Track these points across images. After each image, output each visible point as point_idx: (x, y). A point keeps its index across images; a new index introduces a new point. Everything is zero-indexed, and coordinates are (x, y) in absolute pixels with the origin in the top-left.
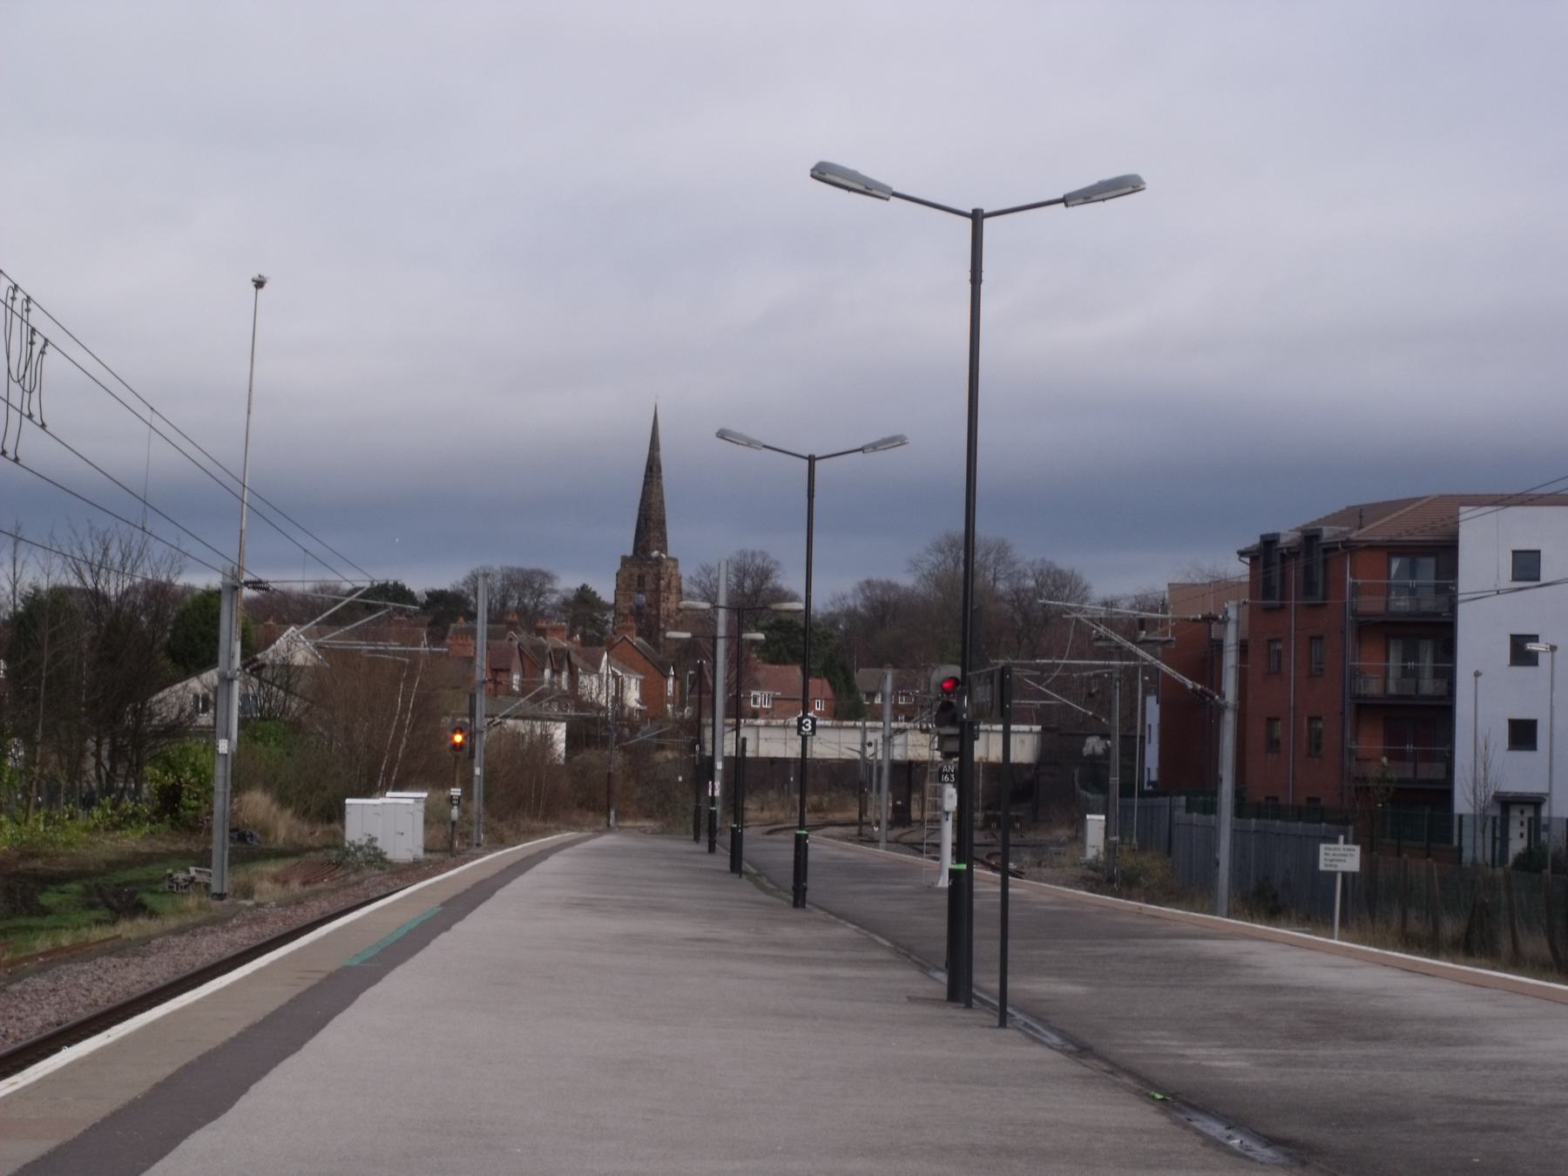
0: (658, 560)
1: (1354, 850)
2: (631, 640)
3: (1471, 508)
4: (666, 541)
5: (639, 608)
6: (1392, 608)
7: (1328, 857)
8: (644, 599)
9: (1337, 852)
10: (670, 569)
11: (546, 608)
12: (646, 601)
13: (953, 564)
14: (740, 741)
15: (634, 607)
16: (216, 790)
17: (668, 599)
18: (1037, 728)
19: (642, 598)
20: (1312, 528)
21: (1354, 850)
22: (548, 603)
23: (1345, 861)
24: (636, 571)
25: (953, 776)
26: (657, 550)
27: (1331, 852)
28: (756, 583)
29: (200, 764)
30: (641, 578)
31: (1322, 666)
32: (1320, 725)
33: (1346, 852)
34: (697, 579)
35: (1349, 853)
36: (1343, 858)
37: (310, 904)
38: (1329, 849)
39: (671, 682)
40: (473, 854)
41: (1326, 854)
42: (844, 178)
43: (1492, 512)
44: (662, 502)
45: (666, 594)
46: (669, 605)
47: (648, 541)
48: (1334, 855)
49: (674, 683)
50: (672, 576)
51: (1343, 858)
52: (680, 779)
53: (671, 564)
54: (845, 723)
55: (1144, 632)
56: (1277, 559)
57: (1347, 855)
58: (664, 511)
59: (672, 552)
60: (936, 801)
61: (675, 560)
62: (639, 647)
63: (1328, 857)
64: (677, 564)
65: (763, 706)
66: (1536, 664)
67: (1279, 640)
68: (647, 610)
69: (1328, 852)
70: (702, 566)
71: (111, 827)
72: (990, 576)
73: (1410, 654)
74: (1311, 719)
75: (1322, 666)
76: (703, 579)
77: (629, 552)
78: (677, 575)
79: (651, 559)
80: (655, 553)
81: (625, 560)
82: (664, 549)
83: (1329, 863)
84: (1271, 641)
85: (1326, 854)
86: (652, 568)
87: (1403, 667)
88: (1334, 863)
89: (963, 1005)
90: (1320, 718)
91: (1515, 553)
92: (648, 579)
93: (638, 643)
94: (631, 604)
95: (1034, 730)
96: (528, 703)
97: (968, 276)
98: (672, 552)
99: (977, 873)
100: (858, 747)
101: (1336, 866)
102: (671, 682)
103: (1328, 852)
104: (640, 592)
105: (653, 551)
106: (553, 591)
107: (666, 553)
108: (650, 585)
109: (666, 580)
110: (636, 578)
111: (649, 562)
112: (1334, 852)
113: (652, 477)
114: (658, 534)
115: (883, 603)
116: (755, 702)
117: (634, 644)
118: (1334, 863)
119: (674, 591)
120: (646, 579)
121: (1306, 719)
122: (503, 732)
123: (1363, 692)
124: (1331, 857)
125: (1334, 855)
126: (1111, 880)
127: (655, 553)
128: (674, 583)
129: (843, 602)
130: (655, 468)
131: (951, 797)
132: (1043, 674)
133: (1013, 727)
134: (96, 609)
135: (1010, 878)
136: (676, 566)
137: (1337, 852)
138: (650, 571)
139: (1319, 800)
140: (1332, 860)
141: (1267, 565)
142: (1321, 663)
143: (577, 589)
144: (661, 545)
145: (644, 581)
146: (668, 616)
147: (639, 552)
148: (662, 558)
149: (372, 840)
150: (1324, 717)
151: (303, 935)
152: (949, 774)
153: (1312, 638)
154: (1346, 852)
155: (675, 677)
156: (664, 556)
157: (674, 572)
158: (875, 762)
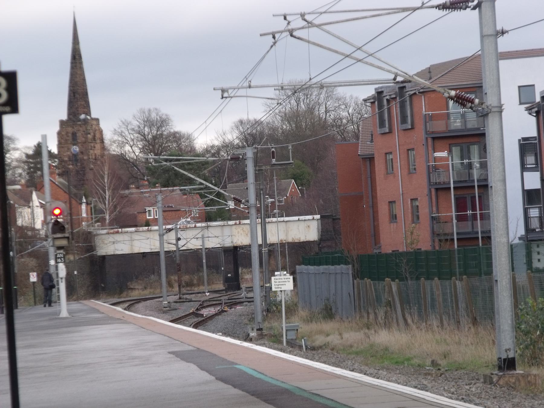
0: (85, 121)
1: (290, 278)
2: (54, 181)
4: (89, 107)
5: (75, 155)
6: (452, 128)
7: (276, 284)
8: (78, 149)
9: (281, 280)
10: (94, 126)
11: (12, 161)
12: (80, 150)
13: (296, 104)
15: (71, 155)
17: (95, 147)
18: (318, 217)
19: (76, 149)
21: (290, 278)
22: (13, 157)
23: (285, 285)
24: (70, 130)
25: (62, 259)
26: (84, 114)
27: (278, 281)
30: (74, 135)
31: (415, 167)
32: (417, 203)
33: (285, 280)
34: (120, 131)
35: (287, 280)
36: (284, 283)
38: (276, 279)
39: (84, 207)
41: (275, 282)
44: (84, 80)
45: (92, 145)
46: (96, 152)
47: (77, 108)
48: (279, 282)
49: (87, 207)
50: (95, 130)
51: (284, 283)
52: (76, 273)
53: (94, 122)
56: (385, 102)
57: (286, 282)
58: (86, 86)
59: (94, 115)
61: (97, 120)
62: (59, 185)
63: (276, 284)
64: (99, 122)
65: (156, 217)
67: (391, 153)
68: (80, 156)
69: (276, 281)
70: (122, 121)
72: (323, 110)
73: (465, 154)
74: (412, 200)
75: (415, 167)
76: (123, 130)
77: (65, 117)
78: (99, 129)
79: (80, 120)
80: (83, 116)
81: (62, 123)
82: (88, 113)
83: (277, 286)
84: (386, 154)
85: (275, 282)
86: (81, 127)
87: (461, 163)
88: (280, 286)
90: (417, 199)
91: (519, 87)
92: (79, 134)
93: (60, 183)
94: (69, 153)
95: (315, 218)
98: (94, 115)
100: (174, 242)
101: (281, 288)
102: (84, 207)
103: (276, 281)
104: (74, 145)
105: (81, 114)
106: (15, 149)
107: (90, 115)
108: (80, 139)
109: (92, 134)
110: (70, 135)
111: (79, 123)
112: (280, 281)
113: (76, 63)
114: (83, 103)
115: (251, 135)
116: (150, 215)
117: (56, 183)
118: (280, 286)
119: (98, 141)
120: (77, 135)
121: (409, 200)
123: (438, 181)
124: (278, 283)
125: (279, 282)
127: (83, 116)
128: (98, 136)
129: (224, 137)
130: (77, 57)
131: (62, 270)
133: (268, 220)
136: (98, 124)
137: (281, 280)
138: (81, 129)
139: (421, 249)
140: (278, 285)
141: (380, 106)
142: (415, 166)
143: (35, 146)
144: (86, 110)
145: (76, 136)
146: (95, 159)
147: (71, 117)
148: (88, 119)
150: (419, 198)
152: (61, 258)
153: (408, 150)
154: (285, 280)
155: (87, 204)
156: (89, 117)
157: (97, 128)
158: (204, 250)
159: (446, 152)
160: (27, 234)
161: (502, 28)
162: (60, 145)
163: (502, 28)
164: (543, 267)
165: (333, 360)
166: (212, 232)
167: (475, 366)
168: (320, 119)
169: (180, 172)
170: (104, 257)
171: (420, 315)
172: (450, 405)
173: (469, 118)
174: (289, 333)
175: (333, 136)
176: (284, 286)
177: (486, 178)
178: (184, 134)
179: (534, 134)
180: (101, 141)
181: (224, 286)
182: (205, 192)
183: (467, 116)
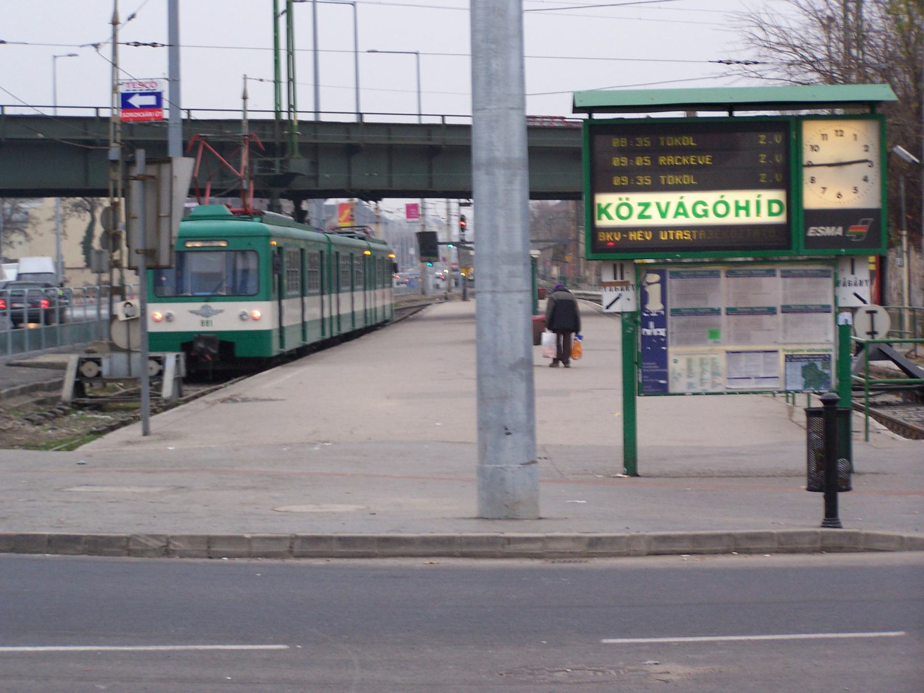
54: (725, 114)
66: (786, 356)
151: (804, 109)
172: (298, 55)
181: (120, 284)
182: (261, 157)
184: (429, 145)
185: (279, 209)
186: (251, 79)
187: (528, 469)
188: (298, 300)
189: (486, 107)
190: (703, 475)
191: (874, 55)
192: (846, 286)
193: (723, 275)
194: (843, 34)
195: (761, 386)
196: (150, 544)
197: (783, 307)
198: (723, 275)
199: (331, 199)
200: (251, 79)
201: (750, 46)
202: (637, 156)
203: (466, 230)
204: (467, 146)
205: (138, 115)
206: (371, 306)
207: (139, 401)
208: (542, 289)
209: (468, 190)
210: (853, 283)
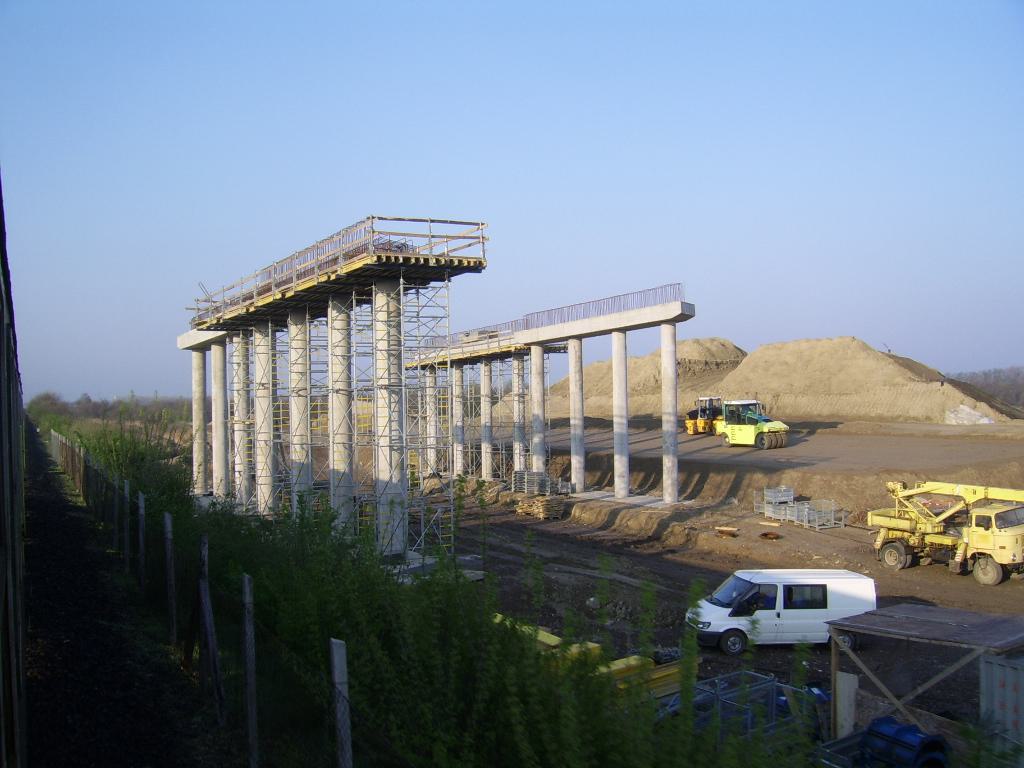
3: (697, 456)
14: (562, 344)
16: (625, 421)
20: (738, 459)
28: (538, 645)
29: (115, 441)
37: (379, 548)
40: (293, 301)
42: (644, 304)
43: (454, 250)
54: (927, 641)
55: (846, 719)
60: (721, 414)
71: (436, 366)
89: (644, 429)
91: (785, 608)
96: (644, 374)
97: (602, 329)
99: (537, 468)
122: (461, 580)
126: (401, 450)
132: (566, 644)
134: (922, 554)
135: (333, 640)
149: (484, 268)
159: (394, 480)
160: (536, 641)
161: (132, 392)
162: (558, 634)
163: (132, 392)
164: (1016, 372)
165: (867, 572)
166: (341, 447)
167: (646, 471)
168: (122, 498)
169: (377, 459)
170: (879, 599)
171: (641, 486)
172: (219, 374)
173: (247, 355)
174: (313, 390)
175: (302, 520)
176: (188, 306)
177: (546, 356)
178: (990, 371)
179: (717, 433)
180: (315, 356)
181: (35, 403)
182: (730, 699)
183: (218, 490)
184: (977, 678)
185: (762, 697)
186: (404, 220)
187: (806, 493)
188: (494, 424)
189: (598, 398)
190: (624, 586)
191: (591, 504)
192: (785, 586)
193: (576, 421)
194: (237, 511)
195: (213, 381)
196: (214, 630)
197: (344, 255)
198: (576, 421)
199: (616, 662)
200: (404, 220)
201: (267, 380)
202: (264, 524)
203: (133, 396)
204: (657, 459)
205: (864, 668)
206: (274, 352)
207: (776, 586)
208: (191, 435)
209: (771, 595)
210: (184, 417)
